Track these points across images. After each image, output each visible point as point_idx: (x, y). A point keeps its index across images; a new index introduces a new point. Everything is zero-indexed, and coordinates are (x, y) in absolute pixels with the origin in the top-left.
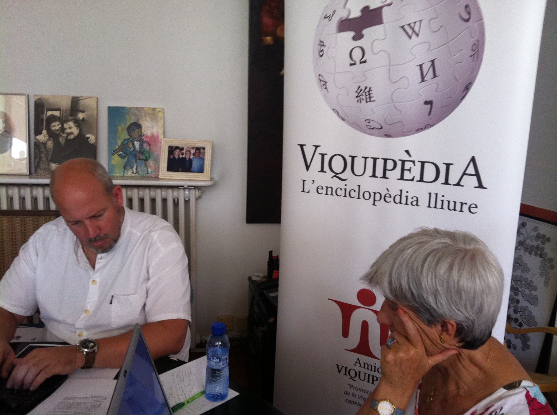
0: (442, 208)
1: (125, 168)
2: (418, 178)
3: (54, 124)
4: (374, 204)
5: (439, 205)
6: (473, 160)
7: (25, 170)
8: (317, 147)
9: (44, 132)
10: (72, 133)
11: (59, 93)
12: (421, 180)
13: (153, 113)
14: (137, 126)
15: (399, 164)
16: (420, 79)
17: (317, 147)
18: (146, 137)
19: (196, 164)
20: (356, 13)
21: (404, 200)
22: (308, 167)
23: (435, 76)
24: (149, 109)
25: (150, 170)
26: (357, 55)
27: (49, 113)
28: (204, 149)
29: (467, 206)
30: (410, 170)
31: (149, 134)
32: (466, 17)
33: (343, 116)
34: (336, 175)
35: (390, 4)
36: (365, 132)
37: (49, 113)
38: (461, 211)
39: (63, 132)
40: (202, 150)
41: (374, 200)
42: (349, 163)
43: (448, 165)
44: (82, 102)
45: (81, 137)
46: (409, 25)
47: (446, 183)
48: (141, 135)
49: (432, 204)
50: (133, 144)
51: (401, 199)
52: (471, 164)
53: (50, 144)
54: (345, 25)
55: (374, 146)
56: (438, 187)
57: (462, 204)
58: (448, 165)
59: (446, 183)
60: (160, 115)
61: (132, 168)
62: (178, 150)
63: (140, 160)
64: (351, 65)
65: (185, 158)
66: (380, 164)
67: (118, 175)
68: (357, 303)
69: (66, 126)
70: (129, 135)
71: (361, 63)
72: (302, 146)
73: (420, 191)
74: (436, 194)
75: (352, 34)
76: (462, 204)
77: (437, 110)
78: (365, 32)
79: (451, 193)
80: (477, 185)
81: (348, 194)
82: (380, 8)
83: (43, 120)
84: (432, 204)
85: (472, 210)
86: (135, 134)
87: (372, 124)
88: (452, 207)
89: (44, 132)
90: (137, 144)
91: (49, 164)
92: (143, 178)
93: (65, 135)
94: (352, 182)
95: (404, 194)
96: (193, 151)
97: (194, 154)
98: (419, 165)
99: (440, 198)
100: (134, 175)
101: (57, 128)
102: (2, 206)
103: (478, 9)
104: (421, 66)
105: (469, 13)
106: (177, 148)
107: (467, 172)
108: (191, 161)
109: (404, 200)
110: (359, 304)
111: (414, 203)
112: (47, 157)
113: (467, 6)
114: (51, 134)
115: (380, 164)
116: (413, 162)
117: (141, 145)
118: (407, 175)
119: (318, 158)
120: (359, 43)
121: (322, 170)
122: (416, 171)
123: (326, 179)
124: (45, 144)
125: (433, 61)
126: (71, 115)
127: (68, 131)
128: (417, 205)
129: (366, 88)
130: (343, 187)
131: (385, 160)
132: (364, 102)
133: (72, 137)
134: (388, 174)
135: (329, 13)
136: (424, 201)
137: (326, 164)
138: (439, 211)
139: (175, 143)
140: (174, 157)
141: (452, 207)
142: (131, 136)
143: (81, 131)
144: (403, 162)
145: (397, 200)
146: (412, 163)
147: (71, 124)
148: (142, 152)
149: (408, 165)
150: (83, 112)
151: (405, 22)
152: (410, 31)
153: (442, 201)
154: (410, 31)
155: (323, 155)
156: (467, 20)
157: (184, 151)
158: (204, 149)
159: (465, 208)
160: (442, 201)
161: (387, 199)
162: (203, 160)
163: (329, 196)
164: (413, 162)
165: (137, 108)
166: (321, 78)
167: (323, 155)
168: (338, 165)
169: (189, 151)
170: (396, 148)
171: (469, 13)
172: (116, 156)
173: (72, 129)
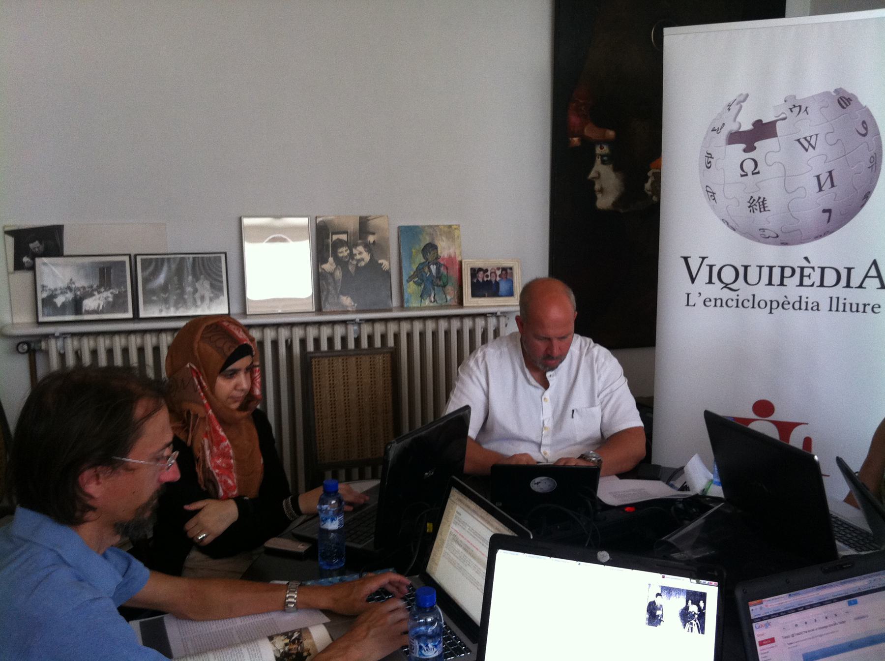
0: (844, 311)
1: (422, 296)
2: (818, 283)
3: (340, 250)
4: (771, 312)
5: (841, 308)
6: (875, 263)
7: (311, 307)
8: (703, 258)
9: (331, 259)
10: (363, 260)
11: (345, 215)
12: (822, 285)
13: (450, 231)
14: (431, 248)
15: (798, 271)
16: (817, 189)
17: (703, 258)
18: (443, 259)
19: (503, 287)
20: (747, 126)
21: (803, 306)
22: (693, 280)
23: (833, 186)
24: (445, 226)
25: (449, 298)
26: (749, 166)
27: (335, 237)
28: (511, 269)
29: (871, 307)
30: (809, 276)
31: (446, 256)
32: (864, 132)
33: (734, 226)
34: (726, 286)
35: (784, 119)
36: (759, 241)
37: (335, 237)
38: (864, 312)
39: (353, 259)
40: (509, 271)
41: (771, 309)
42: (742, 273)
43: (849, 270)
44: (372, 223)
45: (373, 264)
46: (805, 138)
47: (848, 285)
48: (437, 258)
49: (834, 308)
50: (429, 268)
51: (800, 305)
52: (873, 267)
53: (338, 274)
54: (735, 138)
55: (770, 255)
56: (840, 291)
57: (865, 305)
58: (849, 270)
59: (848, 285)
60: (456, 233)
61: (430, 296)
62: (481, 273)
63: (437, 286)
64: (742, 176)
65: (490, 281)
66: (777, 272)
67: (414, 305)
68: (752, 415)
69: (355, 251)
70: (424, 256)
71: (753, 174)
72: (686, 259)
73: (821, 296)
74: (838, 298)
75: (743, 146)
76: (865, 305)
77: (835, 219)
78: (756, 144)
79: (853, 296)
80: (879, 286)
81: (740, 304)
82: (775, 122)
83: (328, 245)
84: (834, 308)
85: (875, 310)
86: (430, 257)
87: (767, 233)
88: (854, 309)
89: (331, 259)
90: (433, 268)
91: (338, 297)
92: (441, 307)
93: (355, 262)
94: (744, 291)
95: (804, 300)
96: (499, 273)
97: (500, 276)
98: (818, 271)
99: (841, 301)
100: (432, 304)
101: (345, 254)
102: (83, 361)
103: (875, 125)
104: (818, 177)
105: (866, 129)
106: (480, 269)
107: (869, 275)
108: (497, 283)
109: (803, 306)
110: (756, 417)
111: (815, 308)
112: (336, 289)
113: (864, 122)
114: (338, 261)
115: (777, 272)
116: (813, 268)
117: (438, 270)
118: (806, 281)
119: (705, 270)
120: (751, 155)
121: (710, 282)
122: (816, 277)
123: (716, 291)
124: (332, 274)
125: (830, 172)
126: (360, 239)
127: (358, 257)
128: (818, 309)
129: (760, 198)
130: (735, 297)
131: (783, 268)
132: (757, 212)
133: (363, 264)
134: (786, 281)
135: (718, 125)
136: (824, 305)
137: (715, 275)
138: (840, 314)
139: (479, 264)
140: (478, 281)
141: (854, 309)
142: (427, 259)
143: (372, 256)
144: (802, 269)
145: (797, 306)
146: (811, 270)
147: (361, 248)
148: (439, 276)
149: (807, 272)
150: (373, 234)
151: (800, 136)
152: (806, 144)
153: (844, 304)
154: (806, 144)
155: (711, 267)
156: (864, 135)
157: (489, 273)
158: (511, 269)
159: (868, 309)
160: (844, 304)
161: (785, 306)
162: (512, 282)
163: (718, 308)
164: (813, 268)
165: (431, 226)
166: (708, 189)
167: (711, 267)
168: (728, 275)
169: (495, 273)
170: (794, 255)
171: (866, 129)
172: (412, 283)
173: (362, 255)
